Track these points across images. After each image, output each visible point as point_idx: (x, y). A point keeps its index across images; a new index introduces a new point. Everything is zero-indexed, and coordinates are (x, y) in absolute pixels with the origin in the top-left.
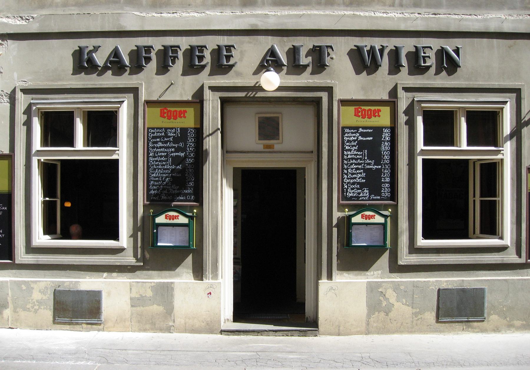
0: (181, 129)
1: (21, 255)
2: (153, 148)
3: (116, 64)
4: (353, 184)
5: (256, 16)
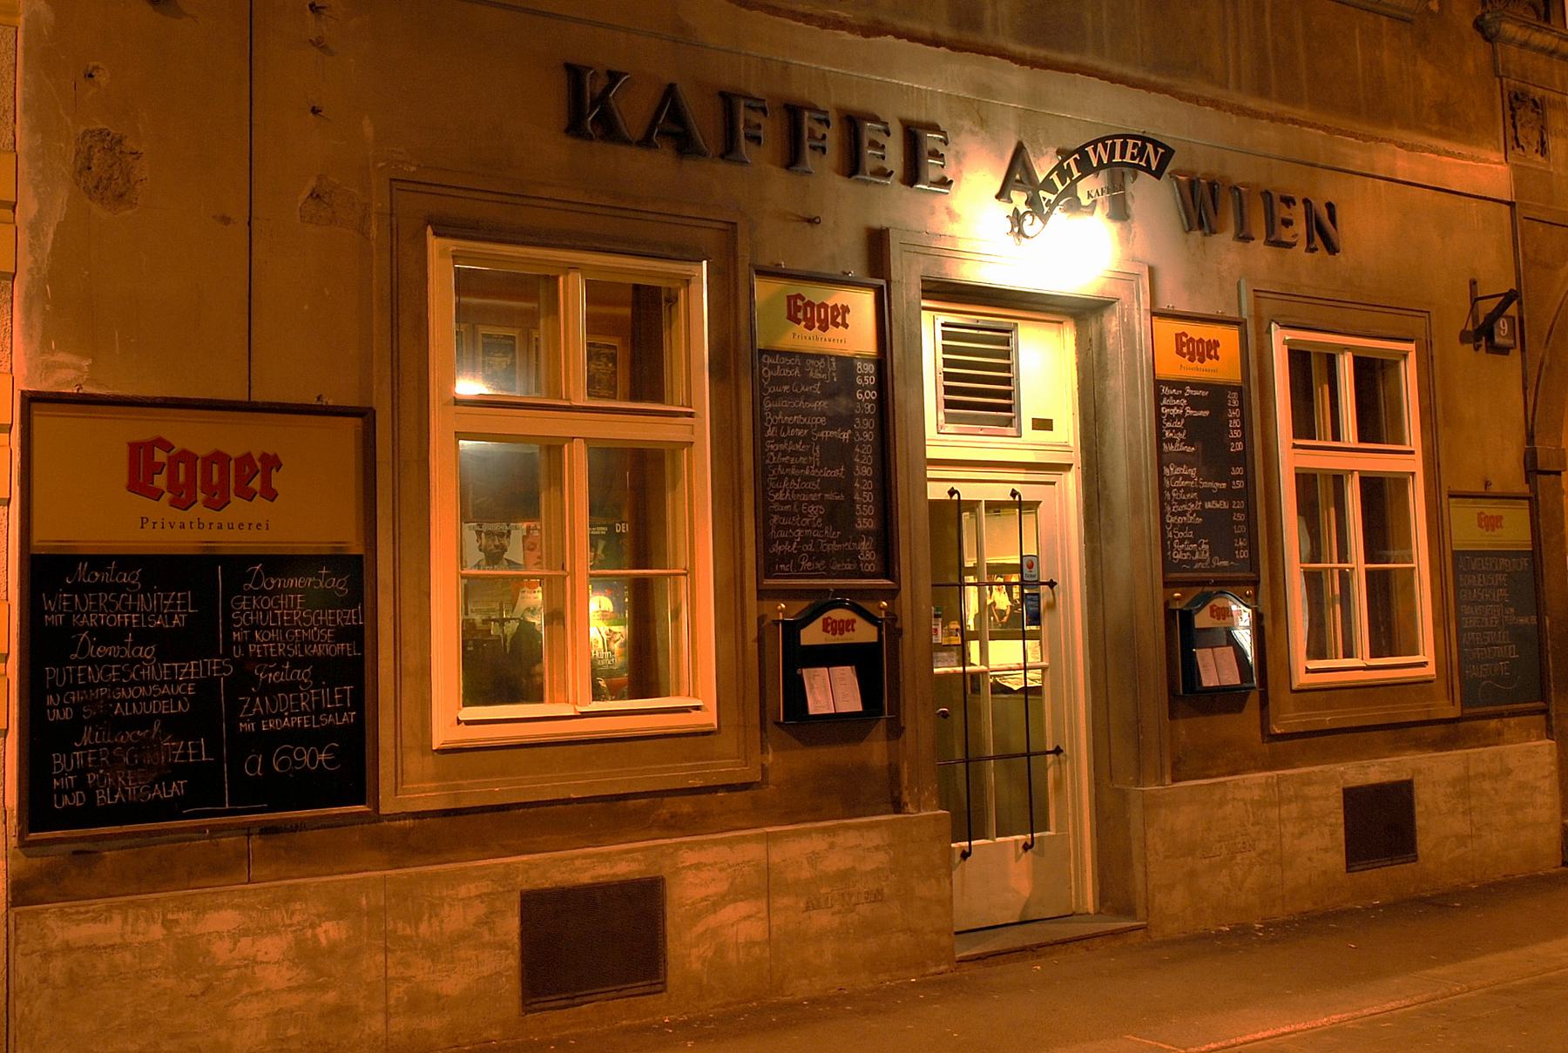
1: (406, 786)
4: (1183, 527)
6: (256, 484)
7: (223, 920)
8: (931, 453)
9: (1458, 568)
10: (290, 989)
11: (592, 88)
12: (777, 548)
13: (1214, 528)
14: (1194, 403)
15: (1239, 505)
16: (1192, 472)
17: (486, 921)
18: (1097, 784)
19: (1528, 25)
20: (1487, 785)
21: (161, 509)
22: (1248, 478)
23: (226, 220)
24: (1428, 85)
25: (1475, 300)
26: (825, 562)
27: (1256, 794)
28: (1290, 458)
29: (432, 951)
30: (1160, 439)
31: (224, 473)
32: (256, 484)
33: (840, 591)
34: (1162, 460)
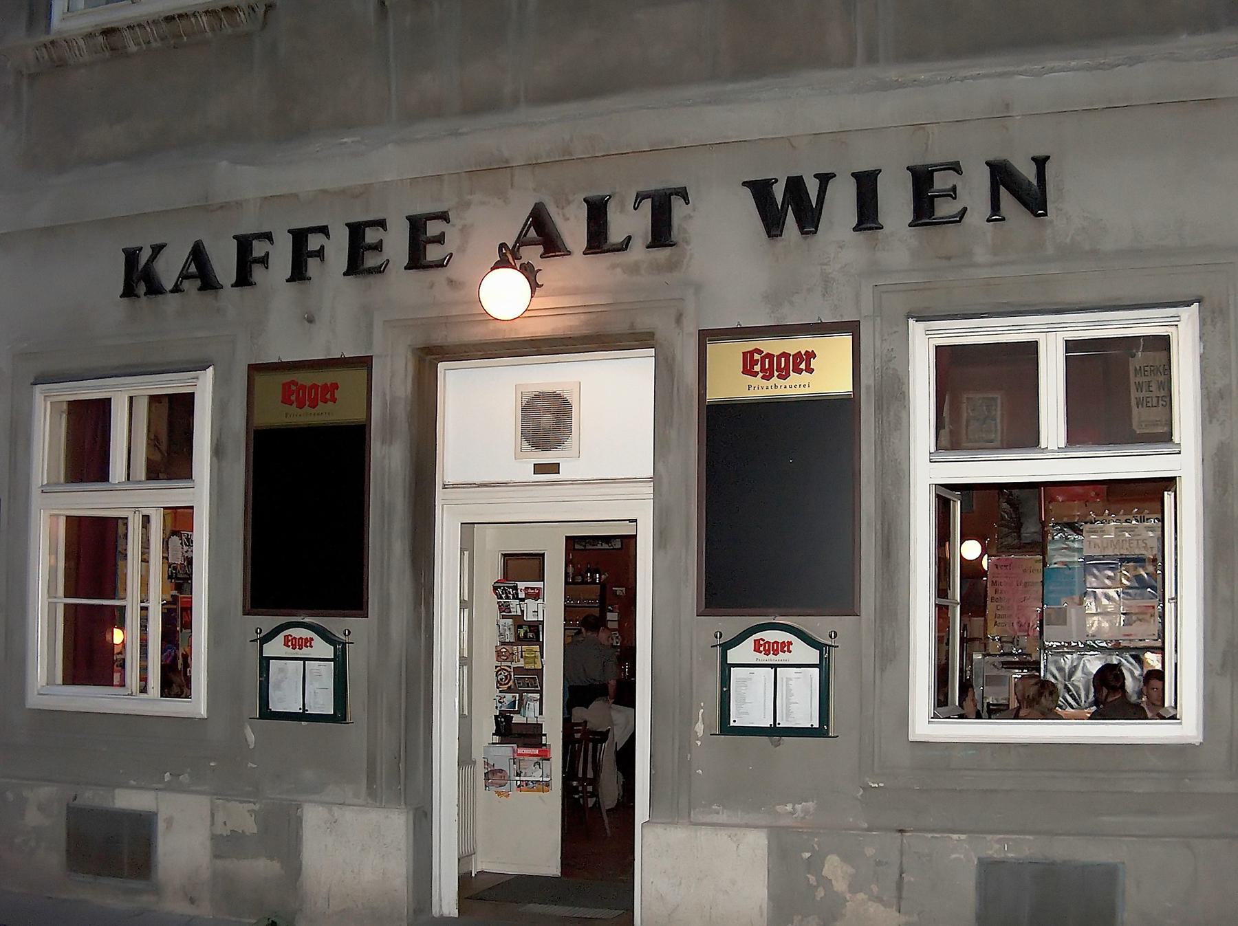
6: (803, 366)
11: (144, 258)
18: (75, 649)
21: (293, 408)
31: (316, 394)
32: (803, 366)
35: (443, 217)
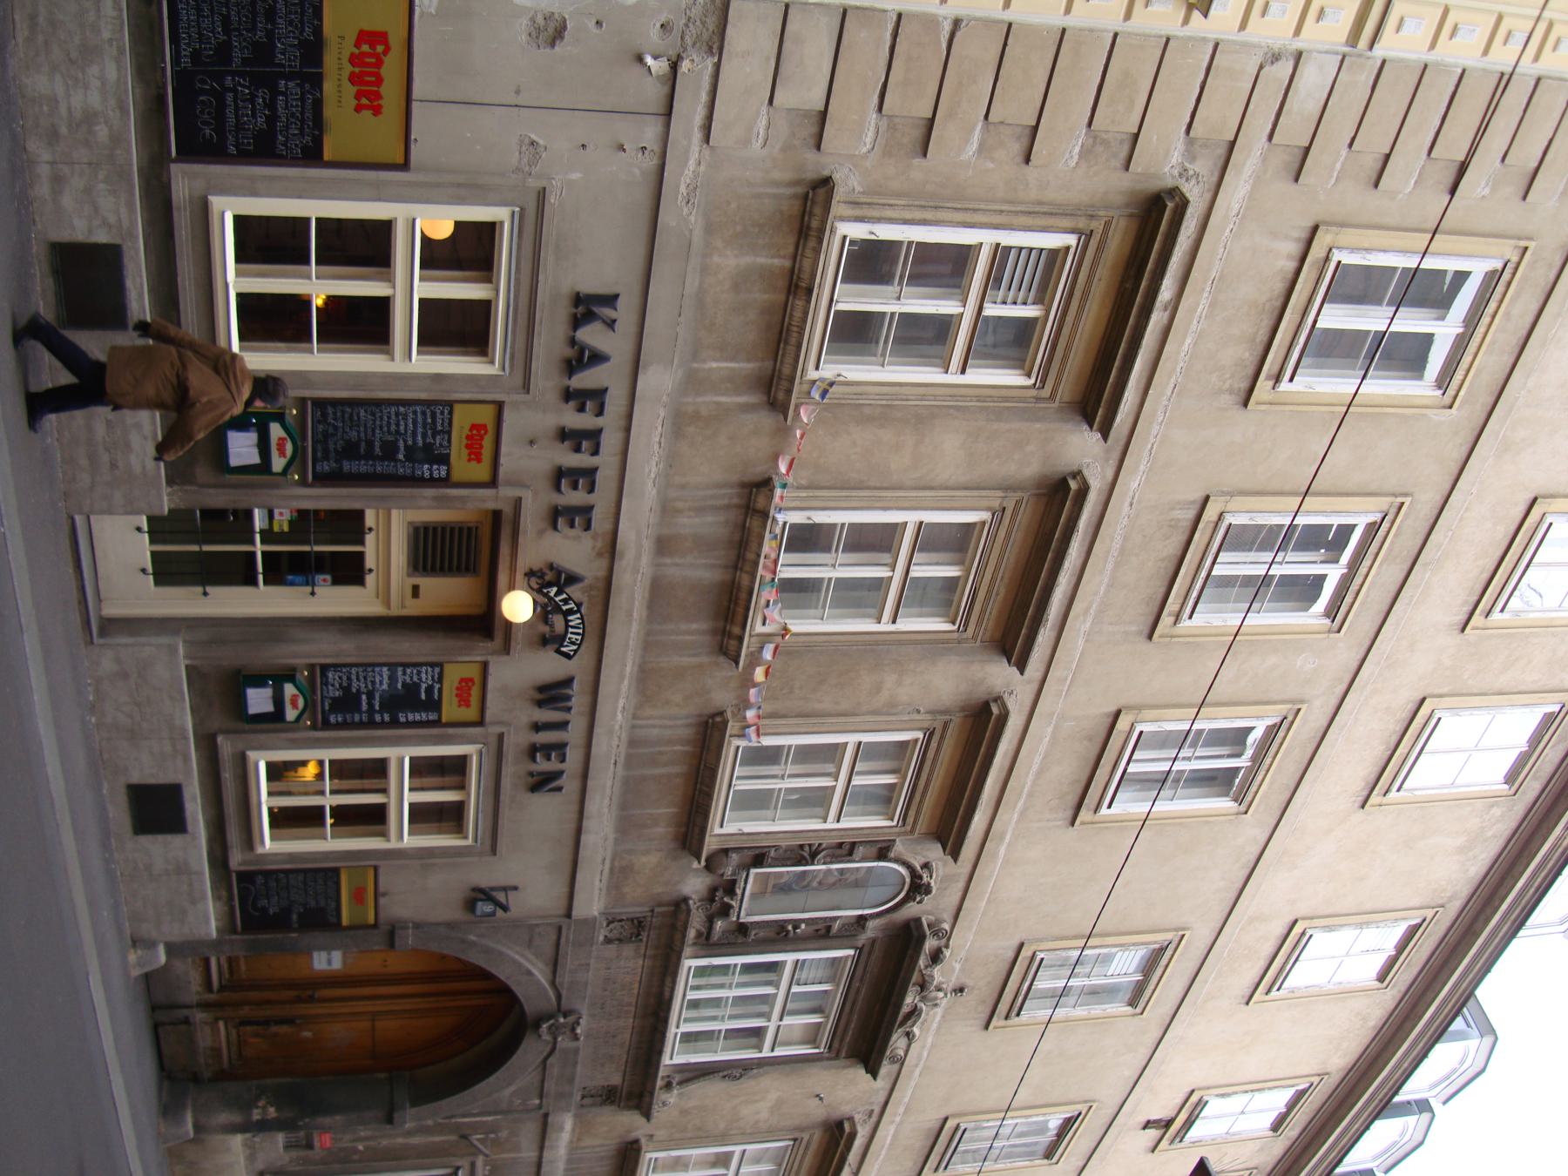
0: (448, 455)
1: (185, 180)
2: (415, 413)
3: (581, 358)
4: (349, 679)
5: (638, 557)
7: (112, 73)
8: (394, 513)
9: (324, 875)
10: (69, 109)
11: (607, 312)
12: (330, 410)
13: (347, 702)
14: (429, 690)
15: (365, 718)
16: (385, 687)
17: (105, 223)
19: (689, 911)
20: (185, 887)
21: (349, 48)
22: (383, 725)
23: (518, 92)
24: (644, 859)
25: (505, 889)
26: (322, 440)
27: (178, 722)
28: (401, 755)
29: (88, 191)
30: (405, 665)
32: (364, 101)
33: (304, 449)
34: (392, 666)
35: (588, 527)
